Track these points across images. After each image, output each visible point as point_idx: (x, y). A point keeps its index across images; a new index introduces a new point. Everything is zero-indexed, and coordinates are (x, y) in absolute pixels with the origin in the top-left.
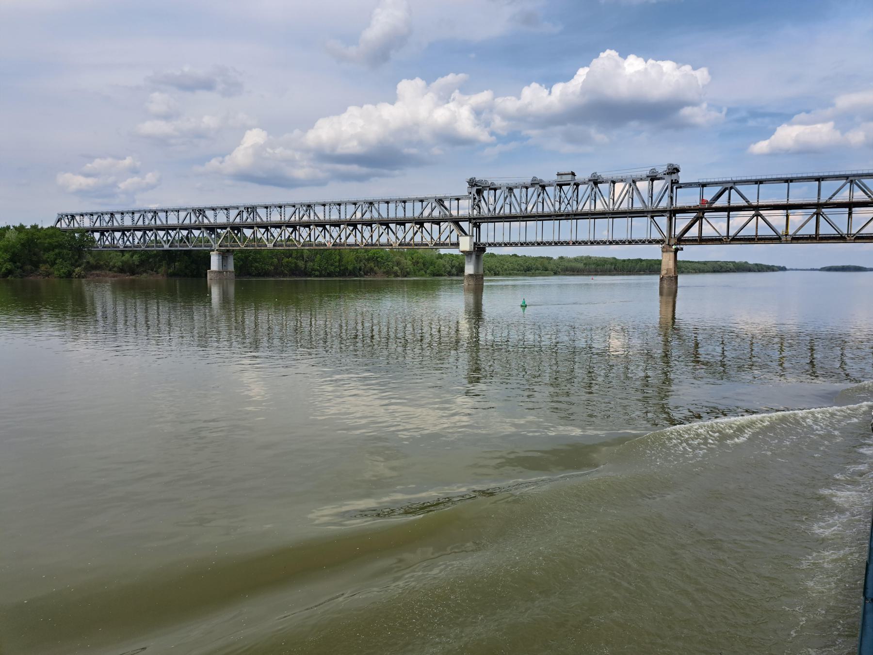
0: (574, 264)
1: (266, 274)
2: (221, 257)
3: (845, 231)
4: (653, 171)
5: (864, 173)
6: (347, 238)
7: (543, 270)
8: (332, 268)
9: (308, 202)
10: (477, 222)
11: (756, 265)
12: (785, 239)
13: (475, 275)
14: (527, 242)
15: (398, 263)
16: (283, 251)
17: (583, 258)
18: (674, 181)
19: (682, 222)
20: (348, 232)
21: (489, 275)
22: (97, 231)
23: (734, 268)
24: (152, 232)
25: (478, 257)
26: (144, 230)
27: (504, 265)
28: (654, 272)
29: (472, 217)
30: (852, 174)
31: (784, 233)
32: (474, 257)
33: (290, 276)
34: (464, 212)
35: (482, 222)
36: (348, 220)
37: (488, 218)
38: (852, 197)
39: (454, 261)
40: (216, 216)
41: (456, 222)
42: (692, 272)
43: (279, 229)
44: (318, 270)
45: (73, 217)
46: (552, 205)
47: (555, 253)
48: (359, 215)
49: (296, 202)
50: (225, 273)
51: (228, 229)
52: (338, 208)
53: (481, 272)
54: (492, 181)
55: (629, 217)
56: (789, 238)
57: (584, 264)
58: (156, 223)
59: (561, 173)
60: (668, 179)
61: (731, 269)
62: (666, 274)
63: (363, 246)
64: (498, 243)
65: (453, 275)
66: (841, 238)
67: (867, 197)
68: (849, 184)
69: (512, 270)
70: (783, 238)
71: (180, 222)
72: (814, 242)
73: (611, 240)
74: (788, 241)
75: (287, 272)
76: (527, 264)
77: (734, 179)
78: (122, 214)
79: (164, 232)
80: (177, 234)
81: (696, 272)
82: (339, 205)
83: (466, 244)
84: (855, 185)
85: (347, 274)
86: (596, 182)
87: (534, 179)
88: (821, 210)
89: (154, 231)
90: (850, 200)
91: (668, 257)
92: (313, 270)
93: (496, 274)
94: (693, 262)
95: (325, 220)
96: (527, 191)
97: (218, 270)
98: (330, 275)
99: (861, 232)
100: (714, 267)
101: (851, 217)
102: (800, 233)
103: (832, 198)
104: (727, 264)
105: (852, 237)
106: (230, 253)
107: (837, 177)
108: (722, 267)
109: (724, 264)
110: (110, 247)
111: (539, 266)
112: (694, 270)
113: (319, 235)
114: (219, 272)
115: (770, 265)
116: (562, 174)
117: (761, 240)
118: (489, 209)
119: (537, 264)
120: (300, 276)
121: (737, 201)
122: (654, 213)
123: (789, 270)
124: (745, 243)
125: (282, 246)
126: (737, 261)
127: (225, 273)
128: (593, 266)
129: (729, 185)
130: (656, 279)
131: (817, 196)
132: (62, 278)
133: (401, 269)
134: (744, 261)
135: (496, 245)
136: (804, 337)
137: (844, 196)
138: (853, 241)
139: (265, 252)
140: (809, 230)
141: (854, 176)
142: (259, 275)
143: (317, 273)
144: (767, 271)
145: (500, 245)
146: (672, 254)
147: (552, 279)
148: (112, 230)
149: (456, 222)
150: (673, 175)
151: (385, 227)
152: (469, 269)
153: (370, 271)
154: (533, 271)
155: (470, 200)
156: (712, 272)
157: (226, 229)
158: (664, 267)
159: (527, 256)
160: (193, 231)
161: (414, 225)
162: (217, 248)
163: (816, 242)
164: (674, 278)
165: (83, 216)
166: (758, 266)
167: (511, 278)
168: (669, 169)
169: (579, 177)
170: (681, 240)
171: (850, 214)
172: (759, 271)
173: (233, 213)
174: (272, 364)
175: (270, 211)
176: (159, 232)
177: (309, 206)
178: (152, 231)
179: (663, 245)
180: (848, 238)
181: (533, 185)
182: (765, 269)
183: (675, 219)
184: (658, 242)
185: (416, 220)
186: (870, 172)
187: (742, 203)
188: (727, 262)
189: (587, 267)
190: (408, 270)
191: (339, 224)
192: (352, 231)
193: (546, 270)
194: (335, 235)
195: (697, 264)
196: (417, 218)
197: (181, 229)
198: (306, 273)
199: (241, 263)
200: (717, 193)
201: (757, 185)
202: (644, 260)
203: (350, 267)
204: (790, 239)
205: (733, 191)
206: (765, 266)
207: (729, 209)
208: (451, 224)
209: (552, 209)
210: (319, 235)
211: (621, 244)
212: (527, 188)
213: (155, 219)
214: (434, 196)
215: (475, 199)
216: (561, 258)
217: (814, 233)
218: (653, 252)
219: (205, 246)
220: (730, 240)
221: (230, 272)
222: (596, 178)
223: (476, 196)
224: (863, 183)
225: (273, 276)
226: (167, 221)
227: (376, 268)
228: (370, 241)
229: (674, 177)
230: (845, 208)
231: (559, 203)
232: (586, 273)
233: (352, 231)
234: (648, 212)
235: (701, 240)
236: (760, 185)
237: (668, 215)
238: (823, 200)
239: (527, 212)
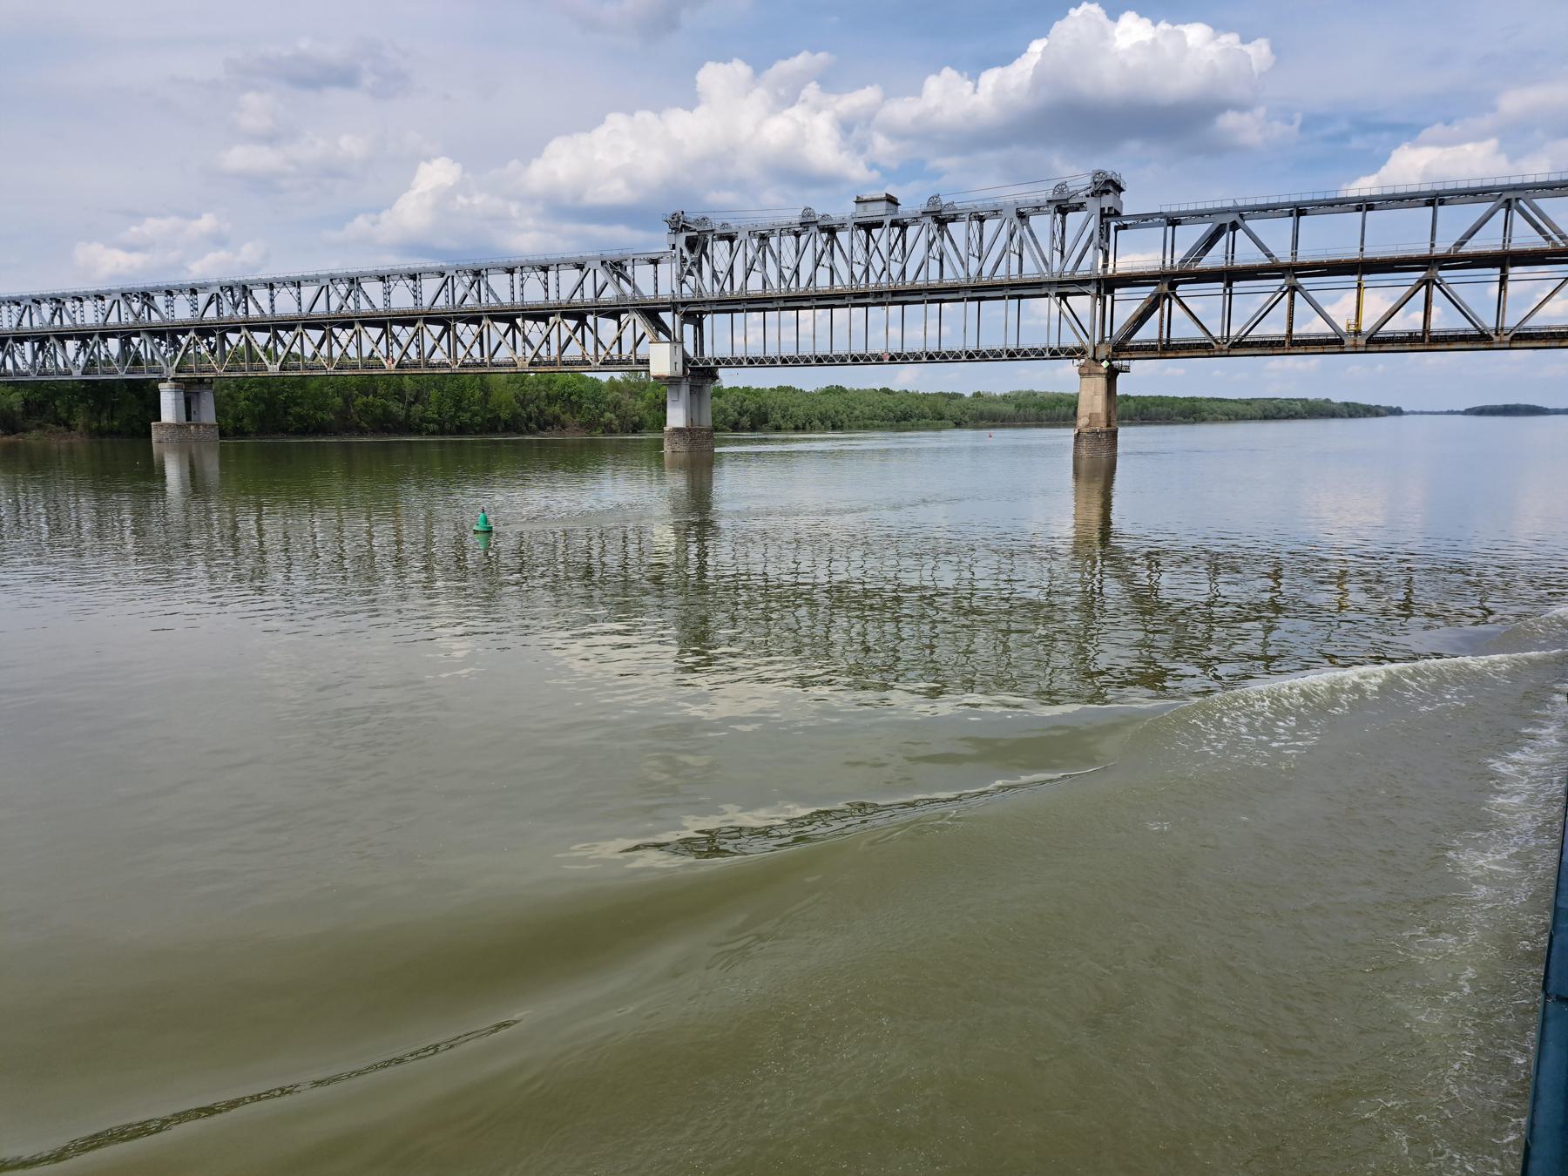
0: (995, 407)
1: (322, 429)
3: (1489, 323)
4: (1061, 188)
6: (562, 350)
7: (934, 418)
8: (465, 417)
9: (143, 286)
10: (693, 313)
11: (1346, 404)
12: (1352, 343)
13: (689, 430)
14: (944, 350)
15: (616, 406)
16: (354, 380)
17: (1021, 395)
18: (1106, 212)
19: (1127, 304)
20: (565, 335)
21: (820, 429)
22: (113, 335)
23: (1303, 411)
24: (350, 332)
25: (696, 391)
26: (41, 339)
27: (855, 408)
28: (1149, 419)
29: (679, 300)
30: (1509, 185)
31: (1352, 328)
32: (685, 389)
33: (374, 432)
34: (665, 292)
35: (707, 313)
36: (426, 310)
37: (1019, 285)
38: (1233, 257)
39: (747, 402)
40: (389, 293)
41: (651, 313)
42: (1221, 420)
43: (477, 326)
44: (434, 421)
45: (246, 290)
46: (963, 264)
47: (810, 380)
48: (589, 294)
49: (319, 273)
50: (192, 427)
51: (192, 334)
52: (542, 278)
53: (707, 421)
55: (1011, 297)
56: (1362, 341)
57: (1016, 407)
58: (247, 313)
60: (1094, 206)
61: (1296, 414)
62: (1087, 426)
63: (457, 367)
64: (912, 354)
65: (743, 429)
66: (1479, 340)
67: (1540, 239)
68: (1503, 211)
69: (869, 419)
70: (1348, 342)
71: (305, 309)
72: (1418, 348)
73: (1055, 346)
74: (1360, 346)
75: (366, 425)
76: (903, 406)
78: (272, 287)
79: (268, 335)
80: (299, 337)
81: (1230, 419)
82: (545, 269)
83: (662, 360)
84: (1515, 211)
85: (500, 428)
86: (942, 221)
87: (807, 212)
88: (1436, 273)
89: (244, 331)
90: (1504, 246)
91: (1093, 388)
92: (423, 420)
93: (834, 428)
94: (1225, 400)
95: (32, 328)
96: (982, 228)
97: (174, 422)
98: (461, 430)
99: (1527, 324)
100: (1266, 410)
101: (1505, 290)
102: (1387, 327)
103: (1464, 243)
104: (1291, 404)
105: (1505, 335)
106: (205, 387)
107: (1551, 188)
108: (1280, 410)
109: (1285, 403)
111: (927, 410)
112: (1227, 415)
113: (500, 343)
114: (178, 426)
115: (1373, 405)
116: (866, 201)
117: (1299, 346)
118: (852, 275)
119: (922, 406)
120: (396, 432)
121: (1247, 254)
122: (1064, 288)
123: (1407, 413)
124: (1548, 345)
125: (355, 367)
126: (1311, 397)
127: (192, 427)
128: (1033, 410)
129: (1227, 219)
131: (1430, 239)
133: (622, 418)
134: (1324, 398)
135: (907, 359)
137: (1488, 241)
138: (1507, 345)
139: (314, 385)
140: (1409, 321)
141: (1515, 188)
142: (303, 432)
143: (432, 426)
144: (1365, 416)
145: (878, 360)
146: (1101, 382)
147: (911, 437)
148: (57, 336)
149: (651, 313)
150: (1105, 197)
152: (676, 417)
153: (555, 422)
154: (914, 421)
155: (674, 265)
156: (1260, 419)
157: (414, 326)
158: (1083, 410)
159: (910, 390)
160: (228, 335)
161: (559, 319)
162: (172, 376)
163: (1422, 348)
164: (1104, 435)
165: (80, 300)
166: (1348, 407)
167: (817, 436)
168: (1096, 183)
169: (906, 209)
170: (1123, 348)
171: (1503, 281)
172: (1351, 416)
173: (430, 286)
175: (522, 279)
176: (256, 334)
177: (477, 273)
178: (239, 332)
179: (1083, 361)
180: (1496, 339)
181: (805, 225)
182: (1362, 412)
183: (1113, 300)
184: (1072, 353)
185: (562, 308)
187: (1259, 259)
188: (1292, 399)
189: (1021, 411)
190: (636, 419)
191: (616, 311)
192: (575, 331)
193: (941, 419)
194: (536, 339)
195: (1234, 403)
196: (564, 304)
197: (306, 326)
198: (408, 427)
199: (262, 407)
200: (1480, 219)
201: (1360, 214)
202: (1133, 398)
204: (1364, 343)
205: (1239, 232)
206: (1362, 406)
207: (1229, 276)
208: (636, 316)
209: (962, 274)
210: (500, 343)
211: (991, 358)
212: (797, 235)
213: (61, 317)
214: (597, 254)
215: (684, 260)
216: (977, 395)
217: (1421, 328)
218: (1062, 378)
219: (104, 373)
221: (205, 425)
222: (938, 209)
223: (686, 254)
224: (1537, 208)
225: (336, 434)
226: (272, 306)
227: (566, 417)
228: (615, 351)
229: (1108, 201)
230: (1352, 274)
231: (938, 263)
232: (1019, 423)
233: (575, 331)
234: (1050, 284)
235: (1167, 349)
236: (1368, 212)
237: (1094, 291)
238: (1443, 247)
239: (1105, 272)
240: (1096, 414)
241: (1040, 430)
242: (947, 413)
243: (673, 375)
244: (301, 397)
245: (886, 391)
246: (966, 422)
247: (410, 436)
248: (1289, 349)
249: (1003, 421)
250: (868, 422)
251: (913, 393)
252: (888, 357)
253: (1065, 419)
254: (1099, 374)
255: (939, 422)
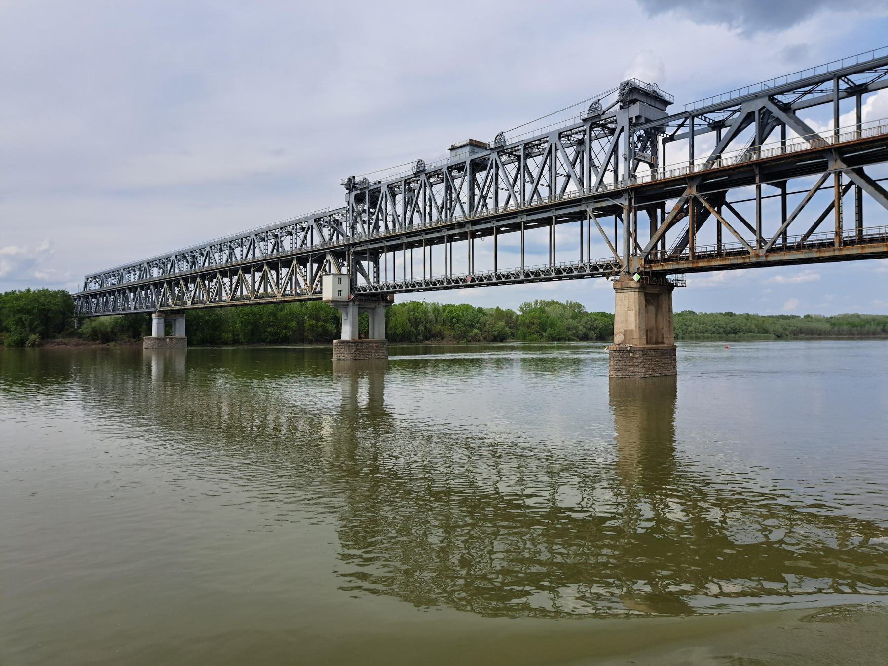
1: (285, 340)
2: (163, 320)
4: (595, 106)
5: (789, 82)
7: (759, 332)
18: (634, 121)
33: (317, 342)
50: (167, 340)
51: (692, 191)
54: (365, 176)
59: (458, 145)
77: (689, 108)
110: (263, 297)
111: (753, 326)
114: (354, 342)
128: (845, 327)
130: (604, 352)
132: (13, 346)
136: (740, 494)
151: (613, 216)
158: (618, 327)
174: (289, 496)
186: (879, 55)
199: (249, 327)
203: (399, 331)
220: (767, 251)
221: (177, 339)
232: (834, 336)
240: (630, 330)
241: (860, 342)
242: (771, 330)
243: (335, 300)
244: (272, 322)
245: (730, 314)
246: (787, 336)
247: (227, 346)
248: (840, 249)
249: (820, 334)
250: (699, 335)
251: (754, 316)
252: (470, 279)
253: (874, 334)
254: (631, 288)
255: (763, 335)
